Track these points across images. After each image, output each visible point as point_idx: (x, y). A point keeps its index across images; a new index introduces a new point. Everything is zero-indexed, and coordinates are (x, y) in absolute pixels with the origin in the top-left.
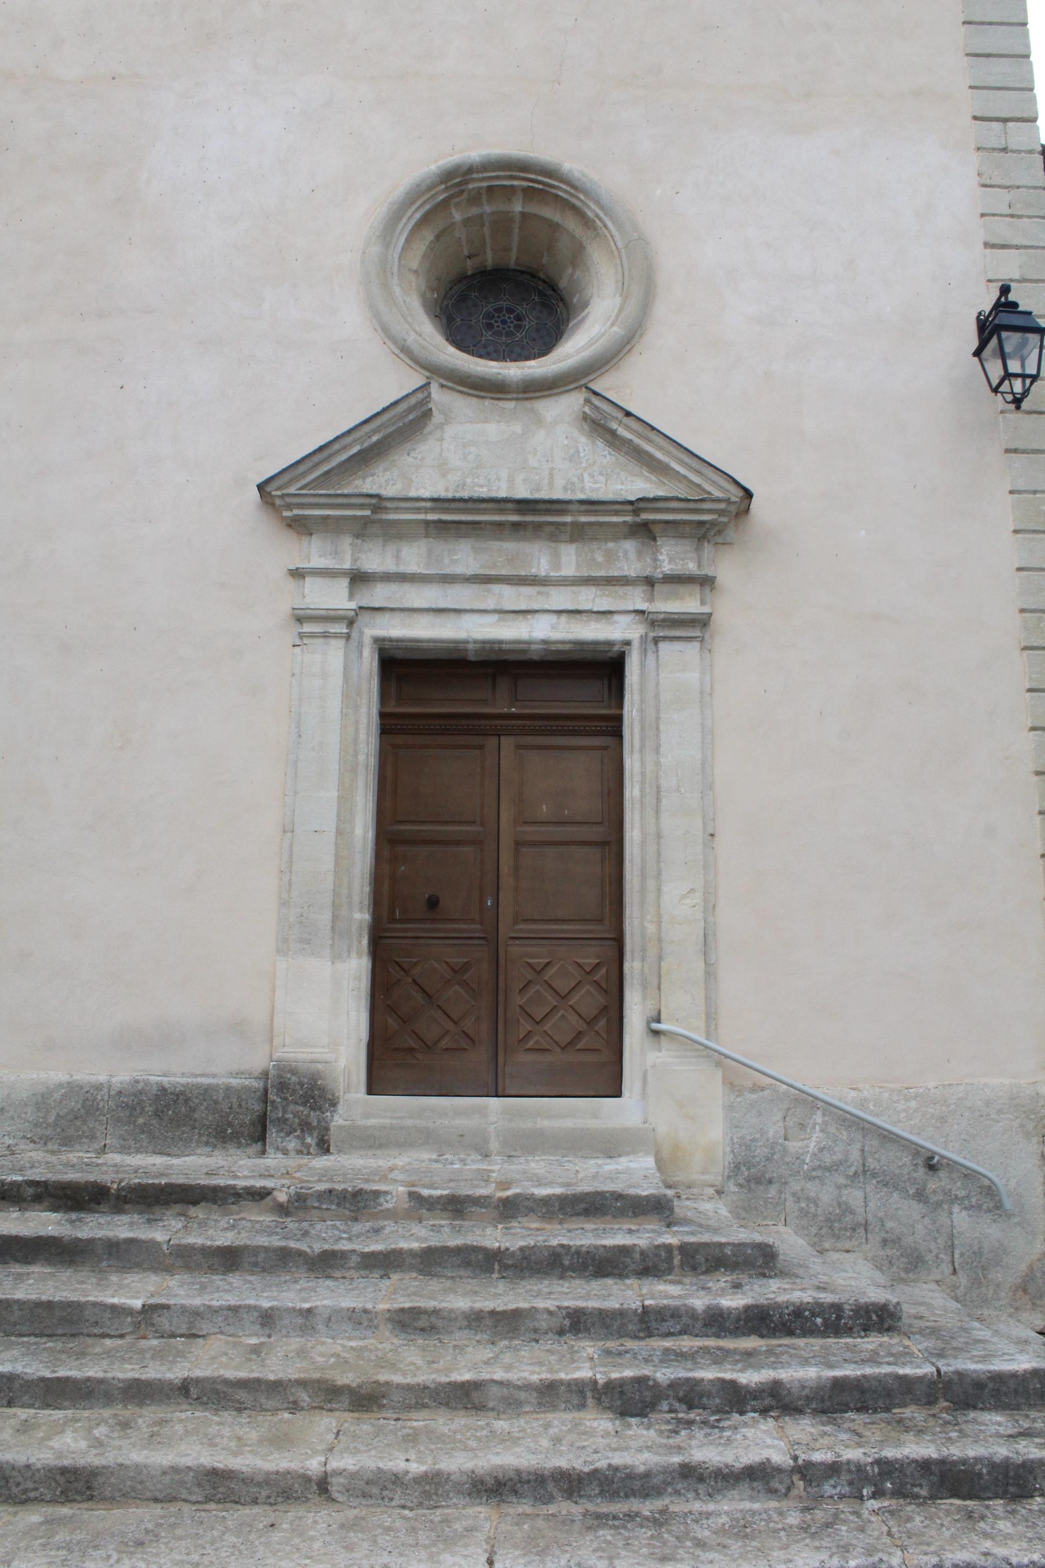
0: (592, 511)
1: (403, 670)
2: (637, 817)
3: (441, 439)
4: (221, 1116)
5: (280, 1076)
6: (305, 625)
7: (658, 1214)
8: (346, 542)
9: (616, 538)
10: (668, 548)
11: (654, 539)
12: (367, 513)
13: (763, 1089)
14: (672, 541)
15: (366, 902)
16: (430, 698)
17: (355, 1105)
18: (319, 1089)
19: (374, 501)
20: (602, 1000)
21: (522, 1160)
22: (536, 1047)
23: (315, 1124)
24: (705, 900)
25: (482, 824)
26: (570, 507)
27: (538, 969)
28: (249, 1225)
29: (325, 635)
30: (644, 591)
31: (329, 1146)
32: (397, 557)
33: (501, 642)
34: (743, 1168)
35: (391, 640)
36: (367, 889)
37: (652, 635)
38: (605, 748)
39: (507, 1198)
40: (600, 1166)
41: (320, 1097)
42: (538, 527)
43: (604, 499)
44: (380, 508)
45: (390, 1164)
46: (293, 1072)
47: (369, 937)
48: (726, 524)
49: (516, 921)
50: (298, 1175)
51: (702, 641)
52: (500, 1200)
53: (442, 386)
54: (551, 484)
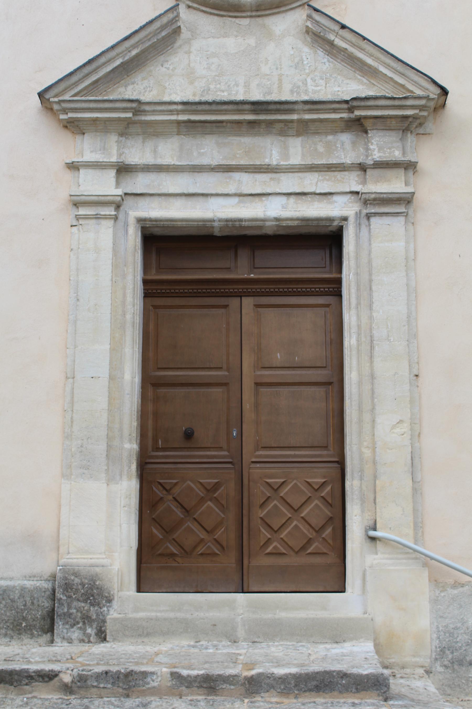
0: (313, 110)
1: (160, 243)
2: (354, 362)
3: (189, 52)
4: (17, 613)
5: (66, 578)
6: (80, 208)
7: (377, 690)
8: (113, 139)
9: (334, 132)
10: (377, 139)
11: (366, 132)
12: (130, 115)
13: (463, 585)
14: (381, 133)
15: (134, 435)
16: (187, 270)
17: (128, 601)
18: (98, 588)
19: (134, 105)
20: (327, 512)
21: (264, 645)
22: (274, 551)
23: (94, 617)
24: (411, 429)
25: (228, 370)
26: (296, 107)
27: (276, 488)
28: (40, 702)
29: (97, 217)
30: (358, 176)
31: (106, 635)
32: (155, 151)
33: (241, 220)
34: (448, 652)
35: (151, 220)
36: (135, 424)
37: (365, 211)
38: (328, 306)
39: (252, 677)
40: (328, 650)
41: (98, 595)
42: (270, 123)
43: (324, 100)
44: (139, 111)
45: (156, 649)
46: (76, 574)
47: (137, 463)
48: (425, 117)
49: (257, 448)
50: (80, 659)
51: (406, 216)
52: (246, 678)
53: (189, 7)
54: (280, 87)
